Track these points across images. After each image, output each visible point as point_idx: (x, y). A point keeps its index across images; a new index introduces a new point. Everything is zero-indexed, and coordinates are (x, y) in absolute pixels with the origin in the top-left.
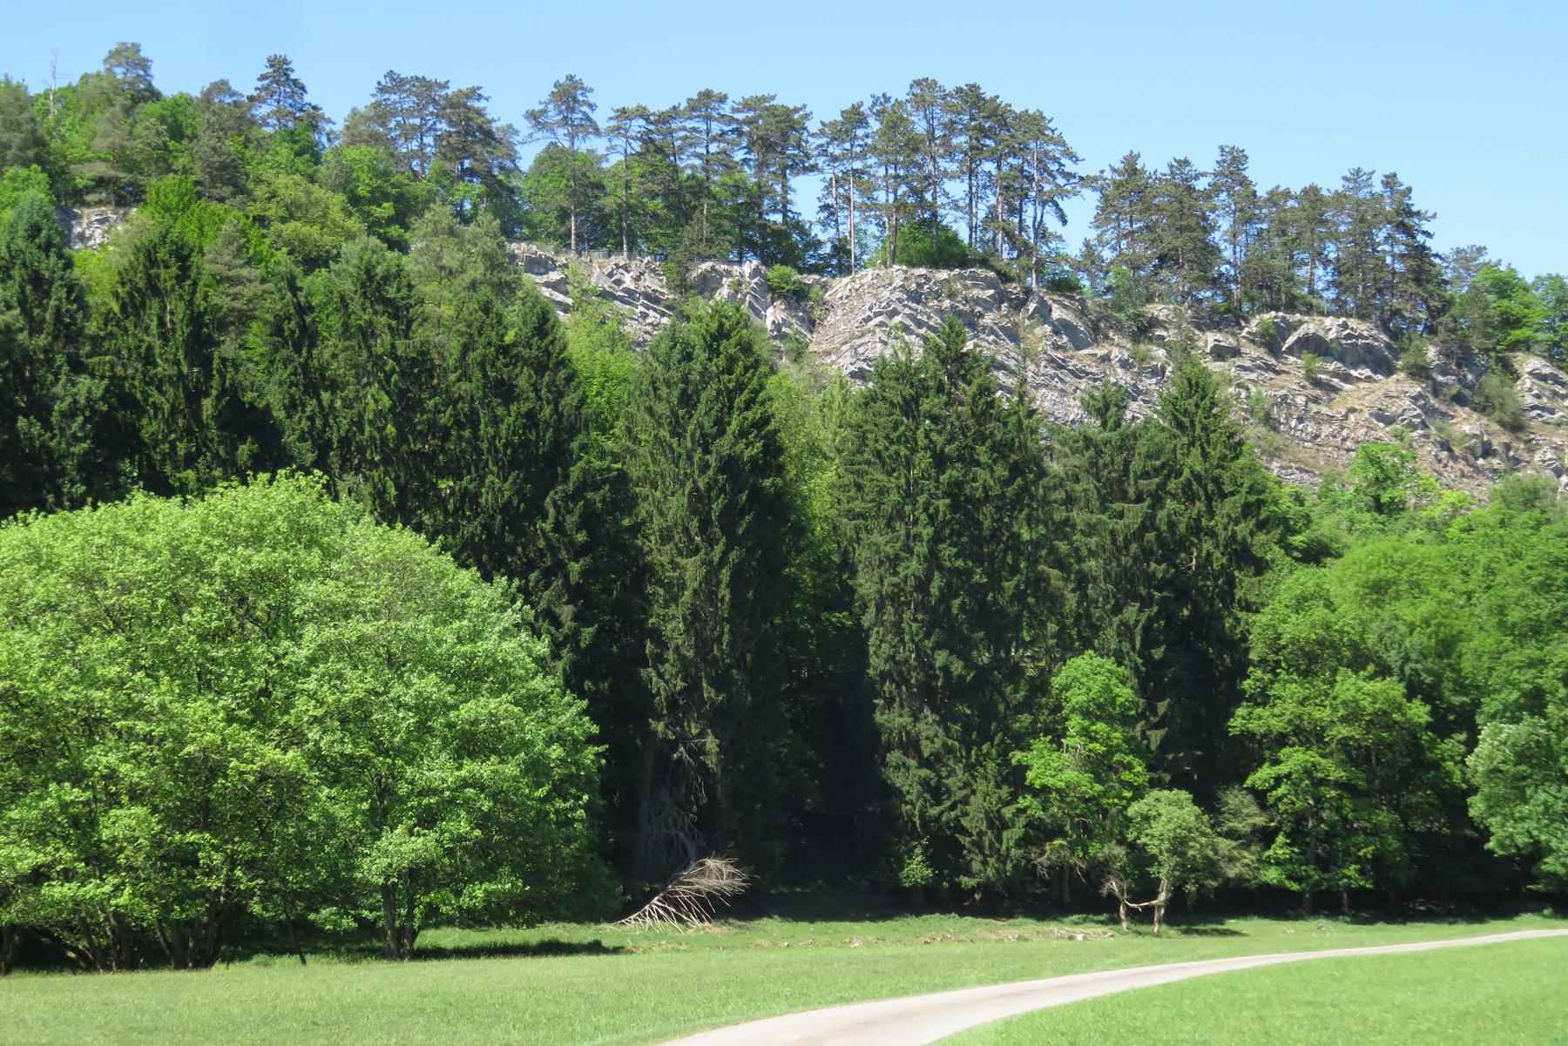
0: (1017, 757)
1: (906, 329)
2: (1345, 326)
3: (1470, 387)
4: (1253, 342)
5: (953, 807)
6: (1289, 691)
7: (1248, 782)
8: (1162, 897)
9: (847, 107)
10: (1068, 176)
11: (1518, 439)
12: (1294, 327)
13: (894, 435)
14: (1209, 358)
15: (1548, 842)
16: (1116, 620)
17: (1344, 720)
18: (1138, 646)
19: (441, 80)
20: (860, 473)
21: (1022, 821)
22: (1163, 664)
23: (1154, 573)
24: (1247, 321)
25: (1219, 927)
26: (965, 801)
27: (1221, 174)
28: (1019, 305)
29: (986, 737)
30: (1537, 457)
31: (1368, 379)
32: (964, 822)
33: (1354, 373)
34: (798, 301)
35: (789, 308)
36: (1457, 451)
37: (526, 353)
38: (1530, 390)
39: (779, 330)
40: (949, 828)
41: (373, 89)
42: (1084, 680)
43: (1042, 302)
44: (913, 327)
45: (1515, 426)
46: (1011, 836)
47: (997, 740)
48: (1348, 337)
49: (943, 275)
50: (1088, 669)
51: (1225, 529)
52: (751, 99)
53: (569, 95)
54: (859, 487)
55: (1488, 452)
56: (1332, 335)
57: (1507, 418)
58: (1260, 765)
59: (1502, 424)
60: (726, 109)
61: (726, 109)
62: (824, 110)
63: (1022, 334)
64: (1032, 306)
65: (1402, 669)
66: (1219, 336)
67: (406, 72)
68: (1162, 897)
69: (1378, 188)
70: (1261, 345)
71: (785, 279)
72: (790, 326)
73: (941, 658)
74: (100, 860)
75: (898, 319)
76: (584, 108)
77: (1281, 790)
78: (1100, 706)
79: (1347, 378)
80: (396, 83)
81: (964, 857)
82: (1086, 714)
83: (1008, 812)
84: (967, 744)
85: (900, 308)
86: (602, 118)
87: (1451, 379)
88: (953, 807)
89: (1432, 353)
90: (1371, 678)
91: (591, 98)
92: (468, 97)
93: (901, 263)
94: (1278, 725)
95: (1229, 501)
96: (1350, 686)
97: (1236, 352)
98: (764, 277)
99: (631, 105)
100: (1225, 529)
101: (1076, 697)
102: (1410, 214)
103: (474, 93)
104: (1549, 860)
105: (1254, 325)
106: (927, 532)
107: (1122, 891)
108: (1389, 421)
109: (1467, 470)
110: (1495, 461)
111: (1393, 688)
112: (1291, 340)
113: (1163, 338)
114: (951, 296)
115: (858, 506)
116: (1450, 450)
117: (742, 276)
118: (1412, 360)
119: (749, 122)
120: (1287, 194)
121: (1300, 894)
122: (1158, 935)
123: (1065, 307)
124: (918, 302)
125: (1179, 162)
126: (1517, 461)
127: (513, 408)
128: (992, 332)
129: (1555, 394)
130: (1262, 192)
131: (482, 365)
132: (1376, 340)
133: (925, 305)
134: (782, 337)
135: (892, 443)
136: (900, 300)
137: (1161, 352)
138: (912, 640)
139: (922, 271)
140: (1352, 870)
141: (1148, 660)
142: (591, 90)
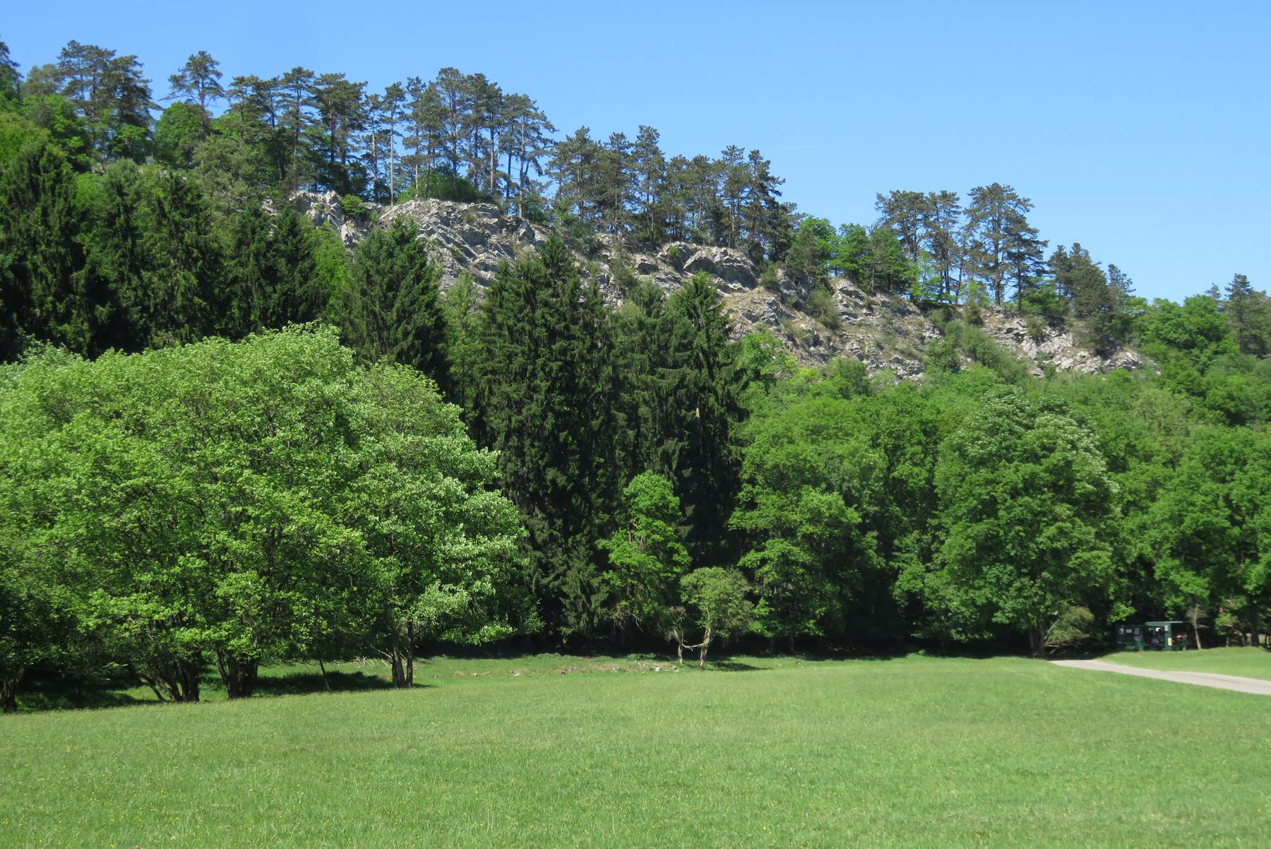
0: (601, 543)
1: (440, 244)
2: (725, 253)
3: (804, 298)
4: (664, 262)
5: (556, 578)
6: (770, 502)
7: (740, 563)
8: (707, 641)
9: (390, 85)
10: (545, 141)
11: (835, 334)
12: (692, 253)
13: (520, 316)
14: (637, 272)
15: (997, 603)
16: (660, 450)
17: (810, 521)
18: (674, 467)
19: (110, 49)
20: (489, 342)
21: (605, 589)
22: (689, 480)
23: (685, 417)
24: (661, 248)
25: (726, 662)
26: (564, 574)
27: (641, 145)
28: (513, 229)
29: (578, 530)
30: (847, 347)
31: (740, 290)
32: (565, 589)
33: (731, 286)
34: (362, 221)
35: (357, 226)
36: (798, 341)
37: (283, 247)
38: (841, 301)
39: (350, 241)
40: (554, 593)
41: (59, 52)
42: (647, 490)
43: (529, 229)
44: (444, 242)
45: (834, 326)
46: (596, 600)
47: (586, 531)
48: (727, 261)
49: (465, 207)
50: (649, 484)
51: (724, 389)
52: (328, 76)
53: (201, 66)
54: (490, 351)
55: (817, 342)
56: (717, 259)
57: (828, 320)
58: (748, 551)
59: (825, 324)
60: (311, 81)
61: (311, 81)
62: (376, 88)
63: (515, 250)
64: (522, 231)
65: (841, 487)
66: (644, 257)
67: (84, 42)
68: (707, 641)
69: (746, 160)
70: (671, 264)
71: (354, 204)
72: (358, 238)
73: (551, 473)
74: (218, 612)
75: (434, 236)
76: (212, 76)
77: (766, 568)
78: (658, 508)
79: (726, 289)
80: (75, 50)
81: (563, 613)
82: (648, 513)
83: (595, 582)
84: (566, 534)
85: (435, 229)
86: (225, 83)
87: (792, 292)
88: (556, 578)
89: (780, 273)
90: (822, 492)
91: (217, 68)
92: (127, 62)
93: (434, 197)
94: (762, 523)
95: (724, 370)
96: (814, 498)
97: (655, 268)
98: (340, 202)
99: (247, 75)
100: (724, 389)
101: (644, 502)
102: (767, 179)
103: (131, 61)
104: (998, 614)
105: (666, 249)
106: (545, 385)
107: (680, 637)
108: (754, 319)
109: (805, 354)
110: (822, 349)
111: (835, 498)
112: (690, 261)
113: (606, 256)
114: (470, 221)
115: (489, 365)
116: (793, 340)
117: (324, 201)
118: (769, 278)
119: (329, 92)
120: (684, 161)
121: (770, 639)
122: (703, 669)
123: (543, 233)
124: (448, 225)
125: (617, 136)
126: (835, 349)
127: (278, 287)
128: (496, 248)
129: (856, 304)
130: (668, 159)
131: (257, 255)
132: (745, 263)
133: (452, 228)
134: (352, 246)
135: (519, 321)
136: (435, 223)
137: (606, 267)
138: (531, 461)
139: (450, 203)
140: (811, 623)
141: (680, 477)
142: (217, 64)
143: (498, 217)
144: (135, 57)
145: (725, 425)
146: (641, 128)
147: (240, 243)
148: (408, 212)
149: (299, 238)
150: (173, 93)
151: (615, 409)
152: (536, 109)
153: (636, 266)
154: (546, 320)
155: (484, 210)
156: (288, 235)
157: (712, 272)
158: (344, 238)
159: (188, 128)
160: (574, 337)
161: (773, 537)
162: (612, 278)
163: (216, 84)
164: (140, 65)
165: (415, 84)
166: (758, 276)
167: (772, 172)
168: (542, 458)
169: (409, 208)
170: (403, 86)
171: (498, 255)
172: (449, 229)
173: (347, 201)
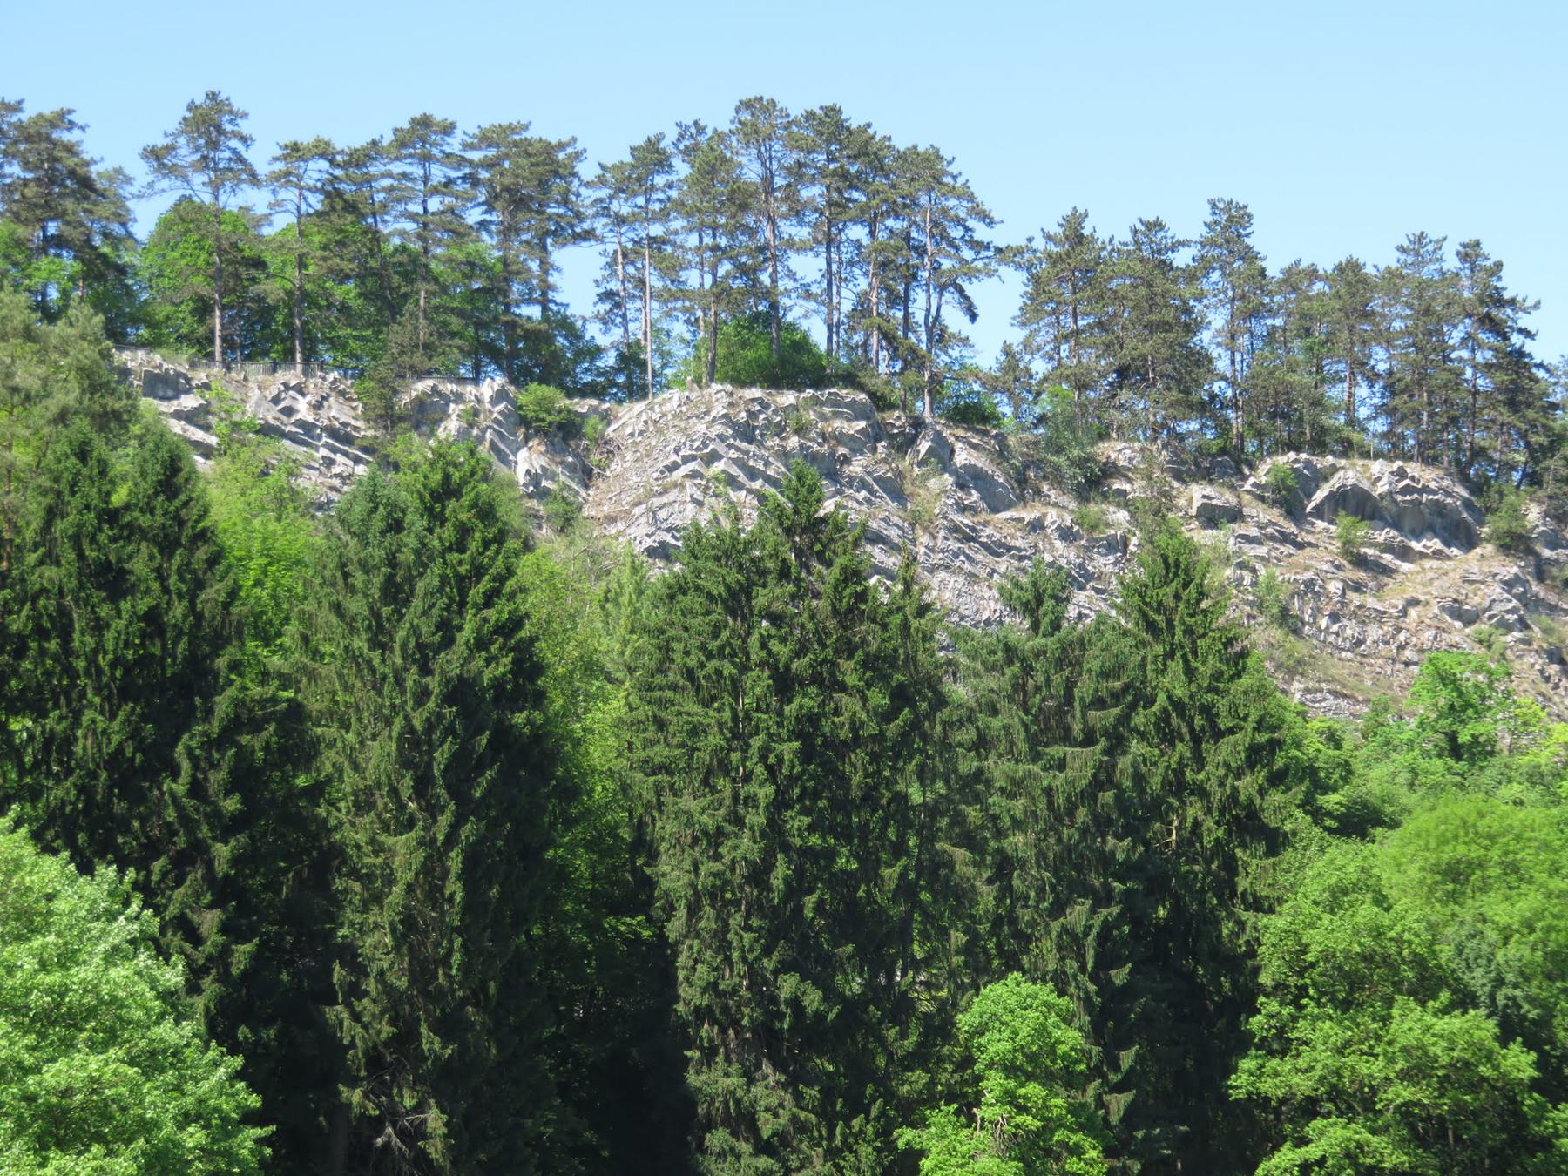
0: (905, 1136)
1: (732, 481)
2: (1401, 474)
4: (1262, 499)
9: (640, 141)
10: (978, 246)
12: (1323, 476)
13: (713, 645)
14: (1195, 524)
16: (1055, 926)
17: (1404, 1076)
18: (1090, 965)
20: (662, 704)
24: (1252, 467)
28: (905, 444)
29: (858, 1106)
31: (1437, 555)
33: (1416, 546)
34: (565, 439)
35: (553, 450)
37: (145, 521)
39: (537, 485)
43: (939, 439)
44: (742, 478)
47: (874, 1112)
48: (1407, 490)
49: (788, 398)
50: (1012, 1002)
51: (1222, 784)
52: (493, 129)
54: (661, 725)
56: (1382, 488)
58: (1277, 1147)
60: (454, 145)
64: (924, 446)
66: (1209, 491)
69: (1451, 263)
70: (1275, 503)
71: (545, 405)
72: (553, 477)
73: (788, 985)
75: (719, 466)
76: (234, 143)
78: (1032, 1058)
79: (1405, 553)
82: (1010, 1070)
85: (721, 449)
86: (262, 158)
90: (1445, 1011)
91: (245, 127)
92: (53, 125)
93: (722, 381)
94: (1303, 1085)
97: (1236, 515)
98: (513, 402)
99: (306, 138)
100: (1222, 784)
101: (996, 1045)
102: (1501, 302)
103: (62, 119)
105: (1262, 474)
106: (765, 793)
108: (1469, 619)
111: (1479, 1026)
112: (1319, 496)
113: (1124, 493)
114: (800, 430)
115: (660, 753)
117: (479, 400)
119: (489, 164)
120: (1313, 274)
123: (974, 447)
125: (1148, 225)
127: (125, 605)
128: (864, 485)
130: (1274, 270)
131: (76, 539)
132: (1448, 494)
133: (761, 444)
134: (542, 494)
135: (710, 656)
136: (722, 438)
137: (1122, 516)
138: (744, 960)
139: (756, 392)
141: (1105, 986)
142: (244, 116)
143: (867, 418)
144: (70, 112)
145: (1231, 866)
146: (1214, 206)
147: (51, 514)
148: (664, 415)
149: (183, 497)
150: (151, 185)
151: (949, 839)
152: (955, 178)
153: (1193, 512)
154: (770, 653)
155: (836, 404)
156: (156, 494)
157: (1372, 518)
158: (521, 477)
159: (204, 256)
160: (843, 688)
161: (1328, 1115)
162: (1134, 541)
163: (241, 160)
164: (83, 129)
165: (693, 138)
166: (1482, 524)
167: (1510, 285)
168: (767, 952)
169: (667, 408)
170: (665, 144)
171: (868, 501)
172: (752, 448)
173: (531, 397)
